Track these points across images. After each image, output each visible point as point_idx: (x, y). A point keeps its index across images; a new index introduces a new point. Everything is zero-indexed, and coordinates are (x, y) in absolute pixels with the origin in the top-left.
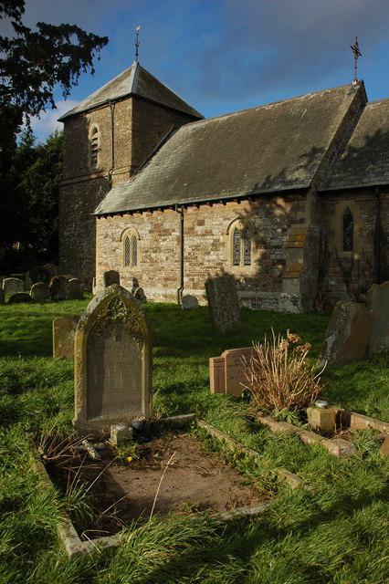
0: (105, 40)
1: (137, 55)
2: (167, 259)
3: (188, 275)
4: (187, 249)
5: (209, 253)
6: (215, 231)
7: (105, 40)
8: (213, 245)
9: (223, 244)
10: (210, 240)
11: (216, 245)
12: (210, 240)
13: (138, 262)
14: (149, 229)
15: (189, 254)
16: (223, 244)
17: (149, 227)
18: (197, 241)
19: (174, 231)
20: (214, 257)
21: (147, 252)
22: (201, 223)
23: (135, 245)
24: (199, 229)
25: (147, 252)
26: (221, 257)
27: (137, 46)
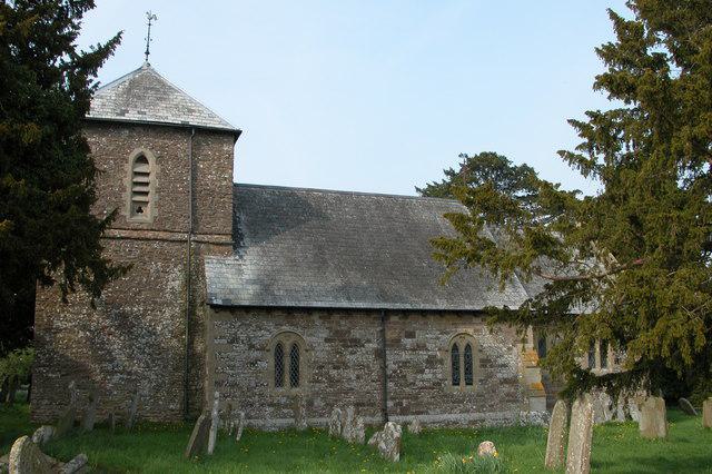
0: (561, 153)
1: (147, 53)
2: (358, 377)
3: (392, 399)
4: (392, 366)
5: (422, 372)
6: (429, 346)
7: (561, 153)
8: (427, 361)
9: (441, 362)
10: (423, 355)
11: (431, 362)
12: (423, 355)
13: (476, 378)
14: (325, 335)
15: (395, 372)
16: (441, 362)
17: (325, 334)
18: (405, 356)
19: (369, 341)
20: (430, 376)
21: (321, 367)
22: (411, 335)
23: (468, 357)
24: (408, 342)
25: (321, 367)
26: (440, 376)
27: (147, 53)
